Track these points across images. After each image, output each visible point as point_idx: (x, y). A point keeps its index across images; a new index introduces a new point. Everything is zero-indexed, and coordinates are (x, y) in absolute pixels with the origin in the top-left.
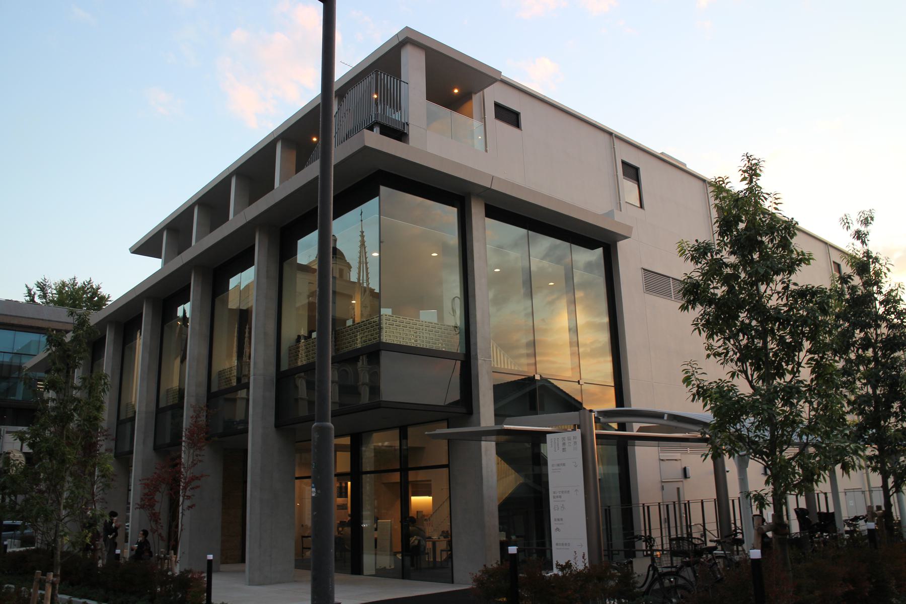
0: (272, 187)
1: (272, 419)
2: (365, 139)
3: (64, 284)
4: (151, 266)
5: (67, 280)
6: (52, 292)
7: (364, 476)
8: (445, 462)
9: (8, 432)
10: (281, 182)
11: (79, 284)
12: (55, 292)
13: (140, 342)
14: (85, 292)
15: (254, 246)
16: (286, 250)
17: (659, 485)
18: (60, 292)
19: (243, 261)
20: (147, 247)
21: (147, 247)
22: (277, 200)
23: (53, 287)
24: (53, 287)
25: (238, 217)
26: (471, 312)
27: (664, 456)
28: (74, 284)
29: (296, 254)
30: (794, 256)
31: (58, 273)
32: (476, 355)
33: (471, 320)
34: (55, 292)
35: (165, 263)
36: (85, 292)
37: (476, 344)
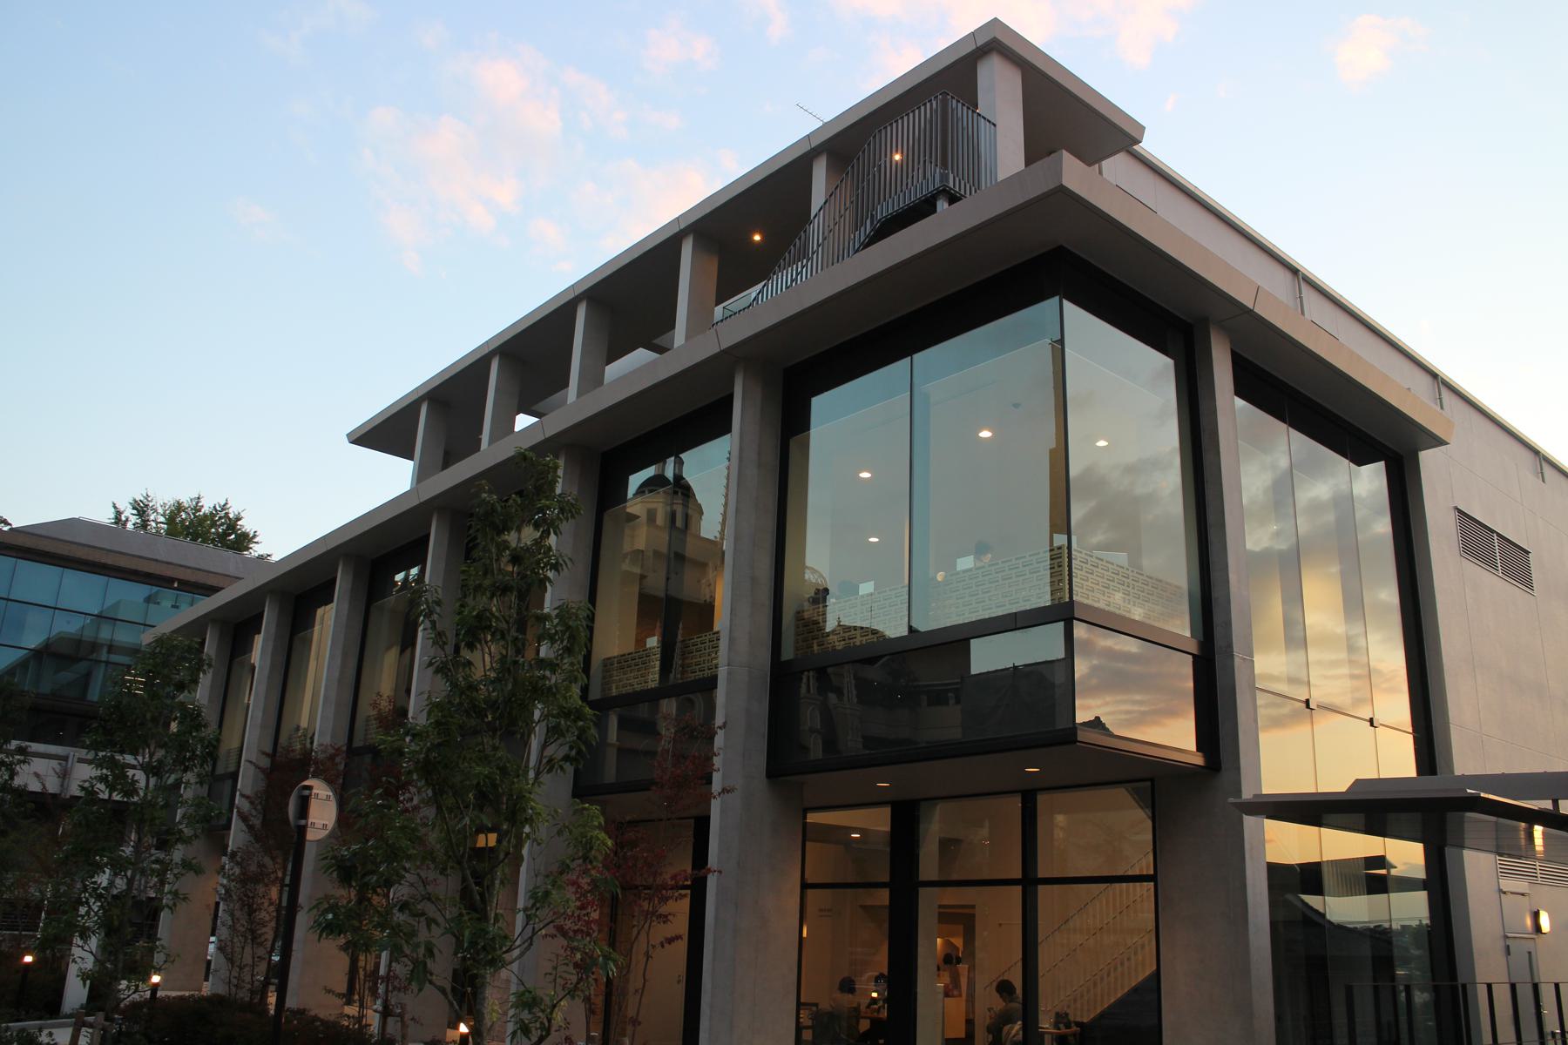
0: (477, 448)
1: (761, 760)
2: (971, 224)
3: (179, 507)
4: (389, 479)
5: (185, 500)
6: (157, 519)
7: (1041, 888)
8: (810, 892)
9: (81, 761)
10: (491, 442)
11: (206, 510)
12: (162, 519)
13: (260, 651)
14: (214, 524)
15: (730, 398)
16: (609, 493)
17: (1500, 944)
18: (171, 519)
19: (708, 421)
20: (385, 434)
21: (385, 434)
22: (244, 591)
23: (160, 511)
24: (160, 511)
25: (690, 341)
26: (1214, 558)
27: (1508, 884)
28: (197, 509)
29: (808, 428)
30: (573, 753)
31: (170, 488)
32: (1230, 646)
33: (1215, 576)
34: (162, 519)
35: (421, 476)
36: (214, 524)
37: (1228, 624)
